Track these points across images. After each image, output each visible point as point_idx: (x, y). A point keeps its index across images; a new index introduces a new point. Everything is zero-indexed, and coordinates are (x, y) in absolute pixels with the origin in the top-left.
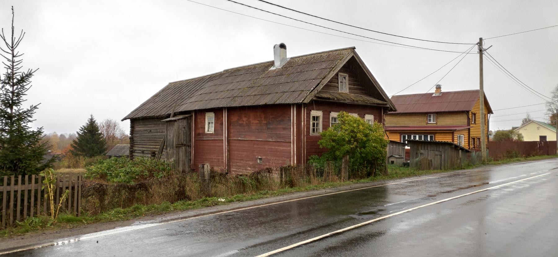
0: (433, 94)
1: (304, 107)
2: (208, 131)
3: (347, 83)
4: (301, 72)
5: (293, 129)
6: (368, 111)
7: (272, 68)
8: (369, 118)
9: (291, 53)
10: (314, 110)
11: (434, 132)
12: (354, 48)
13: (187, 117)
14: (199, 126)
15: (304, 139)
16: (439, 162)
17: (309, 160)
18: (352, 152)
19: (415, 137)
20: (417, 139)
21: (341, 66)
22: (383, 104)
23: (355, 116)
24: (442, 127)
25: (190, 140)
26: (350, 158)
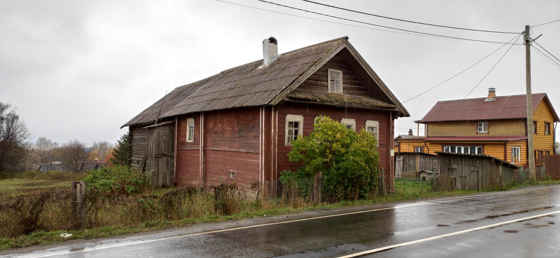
0: (485, 98)
1: (275, 111)
2: (189, 139)
3: (341, 82)
4: (284, 68)
5: (262, 137)
6: (369, 116)
7: (261, 67)
8: (349, 122)
9: (283, 48)
10: (344, 118)
11: (482, 144)
12: (347, 38)
13: (168, 124)
14: (182, 134)
15: (275, 150)
16: (476, 180)
17: (281, 175)
18: (326, 166)
19: (459, 150)
20: (463, 152)
21: (328, 60)
22: (390, 108)
23: (352, 122)
24: (495, 137)
25: (173, 150)
26: (323, 175)
